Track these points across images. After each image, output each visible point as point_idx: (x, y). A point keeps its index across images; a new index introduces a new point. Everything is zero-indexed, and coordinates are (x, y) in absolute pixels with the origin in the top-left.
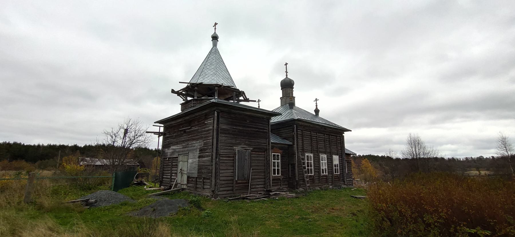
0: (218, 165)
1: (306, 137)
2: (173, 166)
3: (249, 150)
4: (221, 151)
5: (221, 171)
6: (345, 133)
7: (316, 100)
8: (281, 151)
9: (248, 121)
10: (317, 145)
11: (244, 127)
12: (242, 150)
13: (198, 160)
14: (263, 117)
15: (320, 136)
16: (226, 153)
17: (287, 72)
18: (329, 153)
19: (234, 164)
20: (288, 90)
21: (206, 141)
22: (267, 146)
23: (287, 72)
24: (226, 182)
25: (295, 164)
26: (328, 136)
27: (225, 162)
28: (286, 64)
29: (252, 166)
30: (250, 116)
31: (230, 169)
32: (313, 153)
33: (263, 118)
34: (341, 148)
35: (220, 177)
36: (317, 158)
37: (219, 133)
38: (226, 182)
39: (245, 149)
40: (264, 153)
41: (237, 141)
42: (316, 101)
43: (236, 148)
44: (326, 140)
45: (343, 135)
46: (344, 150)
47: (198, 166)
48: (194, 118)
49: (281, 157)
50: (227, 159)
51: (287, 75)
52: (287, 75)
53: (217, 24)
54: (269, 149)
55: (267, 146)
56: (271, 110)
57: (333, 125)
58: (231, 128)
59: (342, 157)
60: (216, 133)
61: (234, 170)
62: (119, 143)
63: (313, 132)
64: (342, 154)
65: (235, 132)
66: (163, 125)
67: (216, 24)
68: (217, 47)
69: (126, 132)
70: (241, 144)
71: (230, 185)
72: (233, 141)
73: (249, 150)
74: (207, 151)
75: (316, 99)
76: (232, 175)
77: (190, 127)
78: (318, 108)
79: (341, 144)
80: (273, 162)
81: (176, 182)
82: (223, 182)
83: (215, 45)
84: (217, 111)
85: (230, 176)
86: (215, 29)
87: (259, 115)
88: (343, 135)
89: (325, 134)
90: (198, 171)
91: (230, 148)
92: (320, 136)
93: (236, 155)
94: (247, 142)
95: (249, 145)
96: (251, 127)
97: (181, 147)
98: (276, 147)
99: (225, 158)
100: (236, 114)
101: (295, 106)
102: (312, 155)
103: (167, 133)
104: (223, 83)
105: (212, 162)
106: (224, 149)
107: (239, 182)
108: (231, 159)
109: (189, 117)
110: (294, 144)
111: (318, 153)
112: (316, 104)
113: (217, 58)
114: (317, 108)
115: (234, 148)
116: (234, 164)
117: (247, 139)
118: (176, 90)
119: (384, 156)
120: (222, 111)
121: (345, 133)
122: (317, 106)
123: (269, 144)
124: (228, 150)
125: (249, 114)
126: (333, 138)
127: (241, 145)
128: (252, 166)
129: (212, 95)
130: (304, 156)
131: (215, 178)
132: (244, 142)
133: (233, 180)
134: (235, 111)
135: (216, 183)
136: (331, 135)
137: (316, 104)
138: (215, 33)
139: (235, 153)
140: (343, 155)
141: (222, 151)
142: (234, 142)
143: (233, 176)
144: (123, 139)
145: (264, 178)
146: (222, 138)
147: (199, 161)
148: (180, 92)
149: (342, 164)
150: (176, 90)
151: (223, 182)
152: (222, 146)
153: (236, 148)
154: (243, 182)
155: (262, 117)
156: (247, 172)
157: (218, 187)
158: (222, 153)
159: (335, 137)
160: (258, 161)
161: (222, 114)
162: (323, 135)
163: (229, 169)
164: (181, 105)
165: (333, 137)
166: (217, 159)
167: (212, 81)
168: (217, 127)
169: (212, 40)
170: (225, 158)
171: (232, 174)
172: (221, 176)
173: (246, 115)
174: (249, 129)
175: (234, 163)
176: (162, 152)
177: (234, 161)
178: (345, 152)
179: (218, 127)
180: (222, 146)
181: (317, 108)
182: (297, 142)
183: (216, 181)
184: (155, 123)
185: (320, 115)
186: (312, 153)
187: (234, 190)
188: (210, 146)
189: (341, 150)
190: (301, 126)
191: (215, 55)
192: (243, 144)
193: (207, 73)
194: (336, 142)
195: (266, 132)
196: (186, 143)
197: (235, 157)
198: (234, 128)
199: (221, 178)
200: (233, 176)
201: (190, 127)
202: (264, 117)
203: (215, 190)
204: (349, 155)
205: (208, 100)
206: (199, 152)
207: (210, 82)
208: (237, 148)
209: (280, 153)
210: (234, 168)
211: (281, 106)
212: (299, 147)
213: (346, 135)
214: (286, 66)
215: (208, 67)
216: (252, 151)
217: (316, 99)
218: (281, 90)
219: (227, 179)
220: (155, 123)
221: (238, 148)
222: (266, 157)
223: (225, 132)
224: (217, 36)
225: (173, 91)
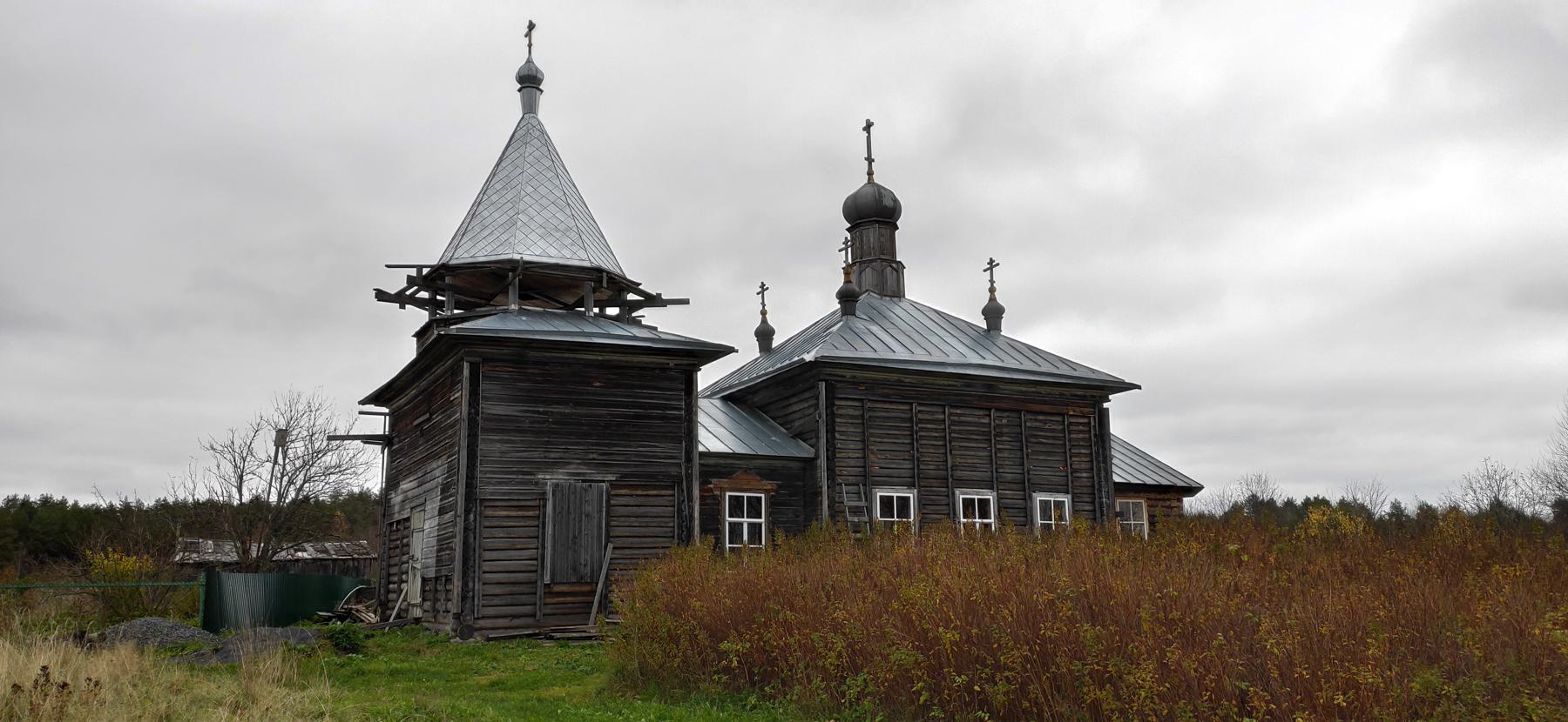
0: (475, 533)
1: (880, 427)
3: (604, 481)
4: (486, 490)
5: (487, 555)
8: (768, 484)
9: (597, 384)
10: (946, 456)
11: (577, 404)
12: (572, 482)
14: (663, 364)
15: (962, 418)
16: (504, 494)
17: (870, 160)
19: (541, 531)
20: (872, 234)
22: (679, 465)
23: (870, 160)
24: (507, 589)
27: (505, 524)
28: (868, 127)
29: (612, 537)
30: (602, 365)
31: (524, 546)
32: (920, 486)
33: (664, 368)
34: (1092, 461)
35: (484, 572)
38: (507, 589)
39: (583, 481)
41: (553, 455)
42: (991, 269)
43: (548, 477)
44: (1001, 434)
45: (1105, 405)
47: (438, 541)
49: (770, 504)
50: (514, 514)
51: (870, 173)
52: (870, 173)
54: (689, 477)
58: (527, 411)
61: (540, 551)
62: (259, 484)
63: (919, 404)
64: (1093, 486)
65: (544, 422)
68: (539, 117)
69: (282, 438)
70: (569, 463)
71: (524, 599)
72: (536, 455)
73: (604, 481)
76: (533, 565)
77: (428, 415)
78: (1000, 300)
80: (730, 523)
81: (405, 600)
82: (498, 590)
83: (530, 107)
84: (470, 359)
85: (523, 569)
87: (645, 359)
88: (1105, 405)
89: (990, 410)
90: (437, 556)
91: (520, 476)
92: (962, 418)
93: (545, 500)
94: (591, 456)
95: (604, 466)
96: (607, 405)
97: (414, 484)
98: (747, 471)
99: (505, 513)
100: (546, 364)
101: (904, 296)
102: (911, 495)
106: (500, 483)
107: (556, 589)
108: (531, 513)
110: (817, 457)
111: (948, 487)
112: (992, 281)
114: (992, 299)
115: (540, 476)
116: (541, 531)
117: (593, 445)
118: (393, 292)
120: (486, 360)
122: (992, 290)
123: (689, 460)
124: (515, 485)
125: (600, 358)
126: (1040, 421)
127: (568, 467)
128: (612, 537)
130: (869, 498)
131: (465, 574)
133: (536, 582)
134: (547, 354)
135: (468, 592)
137: (992, 281)
138: (529, 61)
139: (544, 493)
140: (1100, 491)
141: (490, 488)
142: (541, 458)
143: (536, 571)
144: (276, 462)
146: (490, 446)
148: (416, 288)
151: (498, 590)
152: (490, 472)
153: (548, 477)
154: (577, 589)
155: (657, 364)
156: (592, 556)
157: (476, 603)
158: (492, 493)
159: (1060, 419)
160: (639, 519)
161: (492, 367)
162: (981, 413)
163: (519, 547)
165: (1041, 418)
166: (472, 516)
168: (469, 414)
169: (519, 90)
170: (505, 513)
171: (535, 562)
172: (486, 568)
173: (589, 364)
174: (602, 411)
175: (541, 526)
177: (541, 520)
179: (473, 411)
180: (490, 472)
181: (992, 299)
183: (465, 584)
184: (363, 402)
186: (911, 486)
187: (538, 613)
190: (854, 383)
192: (573, 463)
195: (678, 418)
197: (545, 506)
198: (538, 412)
199: (487, 575)
200: (536, 571)
201: (428, 415)
202: (668, 364)
203: (462, 612)
208: (550, 479)
209: (766, 491)
210: (540, 546)
213: (1115, 404)
214: (869, 133)
216: (613, 485)
219: (512, 580)
220: (363, 402)
221: (556, 477)
222: (678, 504)
223: (502, 425)
225: (381, 296)
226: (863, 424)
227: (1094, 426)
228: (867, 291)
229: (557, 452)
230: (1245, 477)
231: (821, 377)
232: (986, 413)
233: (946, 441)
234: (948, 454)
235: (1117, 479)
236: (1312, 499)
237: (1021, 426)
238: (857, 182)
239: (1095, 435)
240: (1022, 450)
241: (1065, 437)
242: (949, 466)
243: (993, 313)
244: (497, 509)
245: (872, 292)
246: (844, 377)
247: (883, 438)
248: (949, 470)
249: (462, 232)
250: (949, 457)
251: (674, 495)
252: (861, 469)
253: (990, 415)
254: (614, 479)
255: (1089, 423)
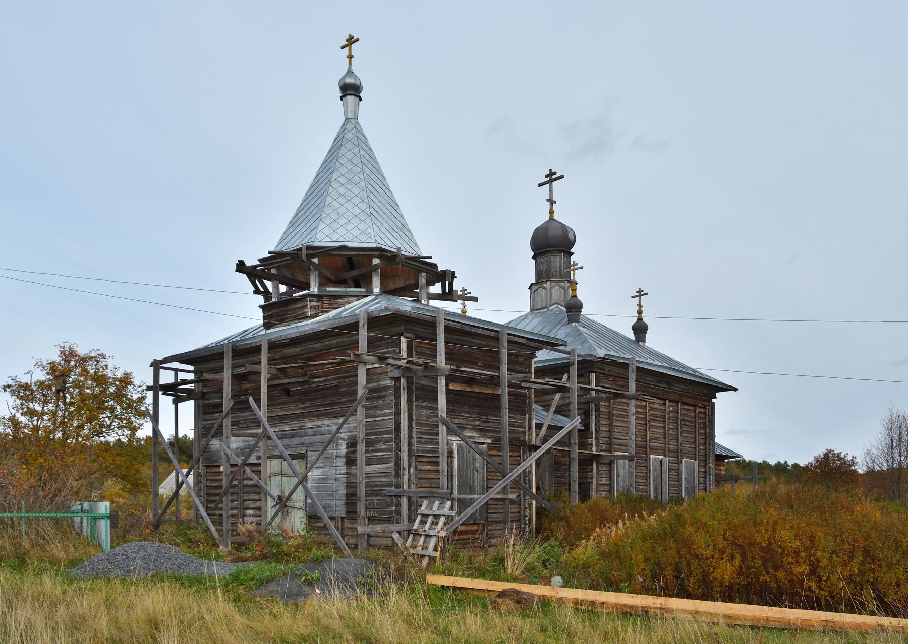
2: (246, 489)
6: (718, 394)
7: (640, 293)
10: (646, 432)
13: (343, 471)
18: (674, 454)
20: (557, 260)
21: (382, 418)
22: (524, 433)
25: (589, 483)
26: (675, 404)
34: (705, 438)
36: (643, 468)
37: (414, 399)
40: (518, 454)
42: (640, 296)
43: (454, 439)
45: (714, 400)
46: (713, 448)
48: (317, 353)
51: (552, 212)
52: (552, 212)
53: (357, 40)
55: (524, 433)
56: (503, 322)
57: (689, 372)
59: (705, 466)
60: (406, 397)
66: (191, 368)
67: (351, 41)
68: (359, 121)
73: (483, 444)
74: (378, 447)
75: (640, 291)
78: (645, 320)
79: (705, 429)
84: (408, 335)
86: (350, 57)
88: (714, 400)
89: (665, 400)
94: (477, 423)
99: (428, 467)
103: (213, 392)
104: (399, 246)
105: (398, 475)
109: (299, 349)
112: (640, 306)
113: (364, 161)
114: (640, 319)
119: (786, 462)
121: (718, 394)
122: (640, 312)
129: (362, 281)
132: (472, 423)
136: (683, 403)
137: (640, 306)
138: (350, 72)
145: (517, 518)
147: (347, 473)
149: (705, 484)
150: (249, 263)
153: (454, 439)
158: (423, 451)
164: (261, 311)
166: (412, 469)
167: (363, 238)
170: (428, 467)
176: (648, 452)
178: (713, 451)
181: (640, 319)
182: (598, 424)
185: (652, 341)
188: (389, 432)
189: (705, 444)
191: (356, 150)
193: (342, 210)
194: (691, 422)
195: (524, 395)
196: (294, 425)
204: (720, 458)
205: (354, 299)
206: (347, 448)
207: (356, 240)
211: (532, 310)
212: (601, 436)
213: (721, 400)
215: (342, 190)
217: (640, 291)
218: (534, 261)
224: (358, 83)
226: (609, 406)
227: (708, 415)
228: (555, 304)
229: (459, 419)
230: (865, 463)
231: (595, 370)
232: (664, 402)
233: (646, 420)
234: (648, 430)
235: (716, 452)
236: (58, 360)
237: (678, 413)
238: (543, 218)
239: (709, 420)
240: (678, 430)
241: (695, 421)
242: (648, 438)
243: (640, 329)
244: (423, 464)
245: (560, 305)
246: (604, 370)
247: (619, 417)
248: (648, 441)
249: (282, 240)
250: (648, 433)
251: (520, 456)
252: (607, 439)
253: (665, 404)
254: (490, 442)
255: (705, 413)
